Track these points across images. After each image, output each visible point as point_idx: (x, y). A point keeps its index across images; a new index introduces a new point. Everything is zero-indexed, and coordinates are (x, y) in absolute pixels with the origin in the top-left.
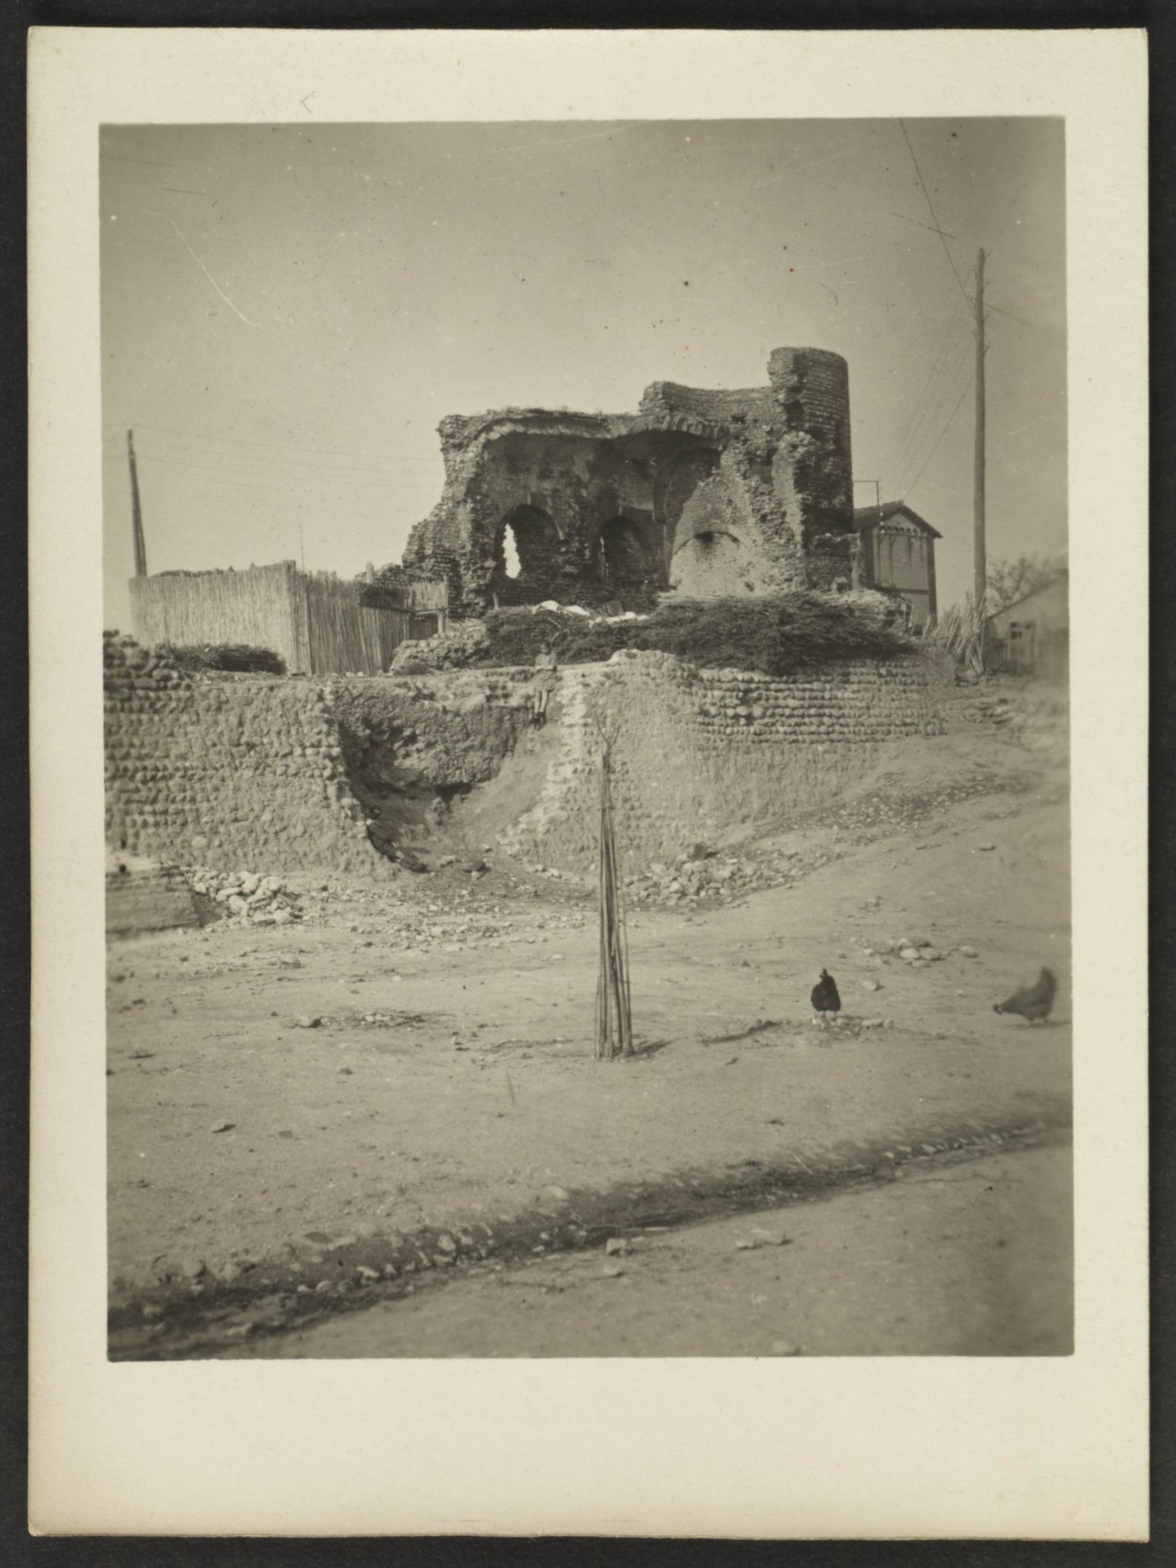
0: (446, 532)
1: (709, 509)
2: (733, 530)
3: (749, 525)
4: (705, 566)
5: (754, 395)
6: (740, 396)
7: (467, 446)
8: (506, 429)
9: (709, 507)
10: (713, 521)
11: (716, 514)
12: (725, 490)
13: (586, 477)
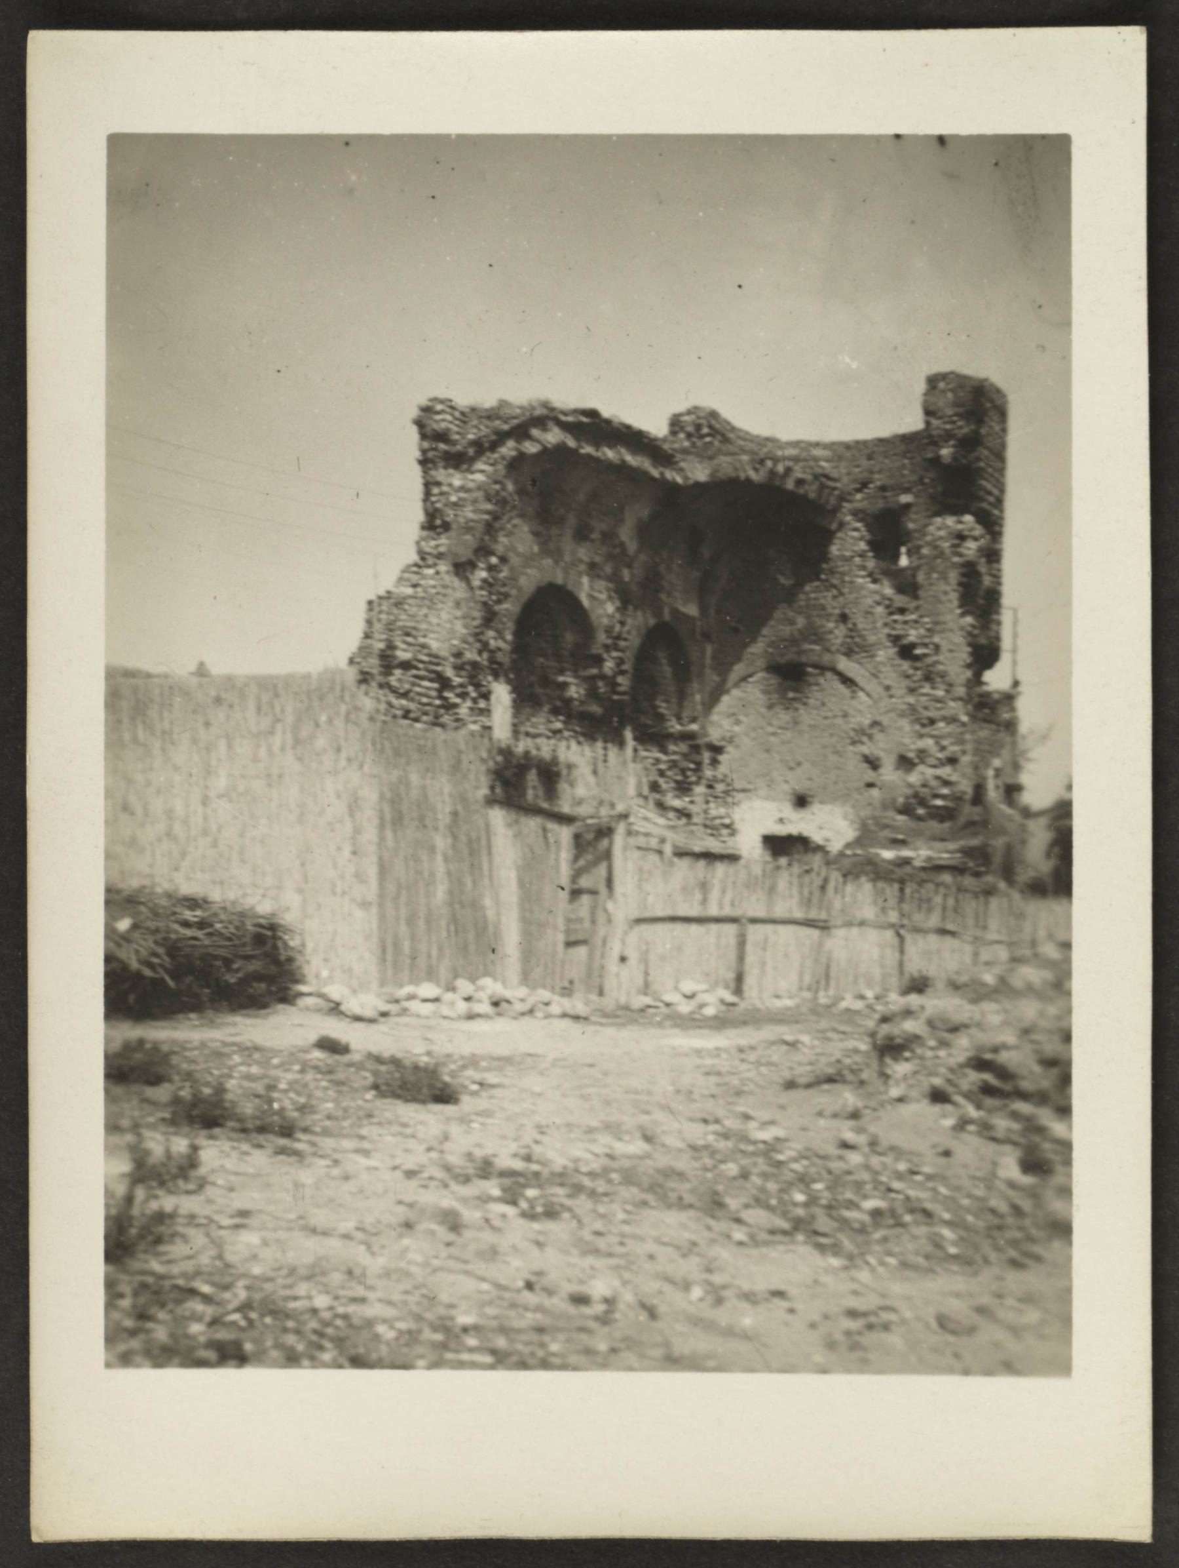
2: (844, 664)
3: (878, 659)
4: (784, 717)
5: (817, 452)
7: (472, 460)
8: (553, 436)
9: (801, 621)
10: (807, 646)
11: (816, 635)
12: (835, 597)
13: (632, 546)
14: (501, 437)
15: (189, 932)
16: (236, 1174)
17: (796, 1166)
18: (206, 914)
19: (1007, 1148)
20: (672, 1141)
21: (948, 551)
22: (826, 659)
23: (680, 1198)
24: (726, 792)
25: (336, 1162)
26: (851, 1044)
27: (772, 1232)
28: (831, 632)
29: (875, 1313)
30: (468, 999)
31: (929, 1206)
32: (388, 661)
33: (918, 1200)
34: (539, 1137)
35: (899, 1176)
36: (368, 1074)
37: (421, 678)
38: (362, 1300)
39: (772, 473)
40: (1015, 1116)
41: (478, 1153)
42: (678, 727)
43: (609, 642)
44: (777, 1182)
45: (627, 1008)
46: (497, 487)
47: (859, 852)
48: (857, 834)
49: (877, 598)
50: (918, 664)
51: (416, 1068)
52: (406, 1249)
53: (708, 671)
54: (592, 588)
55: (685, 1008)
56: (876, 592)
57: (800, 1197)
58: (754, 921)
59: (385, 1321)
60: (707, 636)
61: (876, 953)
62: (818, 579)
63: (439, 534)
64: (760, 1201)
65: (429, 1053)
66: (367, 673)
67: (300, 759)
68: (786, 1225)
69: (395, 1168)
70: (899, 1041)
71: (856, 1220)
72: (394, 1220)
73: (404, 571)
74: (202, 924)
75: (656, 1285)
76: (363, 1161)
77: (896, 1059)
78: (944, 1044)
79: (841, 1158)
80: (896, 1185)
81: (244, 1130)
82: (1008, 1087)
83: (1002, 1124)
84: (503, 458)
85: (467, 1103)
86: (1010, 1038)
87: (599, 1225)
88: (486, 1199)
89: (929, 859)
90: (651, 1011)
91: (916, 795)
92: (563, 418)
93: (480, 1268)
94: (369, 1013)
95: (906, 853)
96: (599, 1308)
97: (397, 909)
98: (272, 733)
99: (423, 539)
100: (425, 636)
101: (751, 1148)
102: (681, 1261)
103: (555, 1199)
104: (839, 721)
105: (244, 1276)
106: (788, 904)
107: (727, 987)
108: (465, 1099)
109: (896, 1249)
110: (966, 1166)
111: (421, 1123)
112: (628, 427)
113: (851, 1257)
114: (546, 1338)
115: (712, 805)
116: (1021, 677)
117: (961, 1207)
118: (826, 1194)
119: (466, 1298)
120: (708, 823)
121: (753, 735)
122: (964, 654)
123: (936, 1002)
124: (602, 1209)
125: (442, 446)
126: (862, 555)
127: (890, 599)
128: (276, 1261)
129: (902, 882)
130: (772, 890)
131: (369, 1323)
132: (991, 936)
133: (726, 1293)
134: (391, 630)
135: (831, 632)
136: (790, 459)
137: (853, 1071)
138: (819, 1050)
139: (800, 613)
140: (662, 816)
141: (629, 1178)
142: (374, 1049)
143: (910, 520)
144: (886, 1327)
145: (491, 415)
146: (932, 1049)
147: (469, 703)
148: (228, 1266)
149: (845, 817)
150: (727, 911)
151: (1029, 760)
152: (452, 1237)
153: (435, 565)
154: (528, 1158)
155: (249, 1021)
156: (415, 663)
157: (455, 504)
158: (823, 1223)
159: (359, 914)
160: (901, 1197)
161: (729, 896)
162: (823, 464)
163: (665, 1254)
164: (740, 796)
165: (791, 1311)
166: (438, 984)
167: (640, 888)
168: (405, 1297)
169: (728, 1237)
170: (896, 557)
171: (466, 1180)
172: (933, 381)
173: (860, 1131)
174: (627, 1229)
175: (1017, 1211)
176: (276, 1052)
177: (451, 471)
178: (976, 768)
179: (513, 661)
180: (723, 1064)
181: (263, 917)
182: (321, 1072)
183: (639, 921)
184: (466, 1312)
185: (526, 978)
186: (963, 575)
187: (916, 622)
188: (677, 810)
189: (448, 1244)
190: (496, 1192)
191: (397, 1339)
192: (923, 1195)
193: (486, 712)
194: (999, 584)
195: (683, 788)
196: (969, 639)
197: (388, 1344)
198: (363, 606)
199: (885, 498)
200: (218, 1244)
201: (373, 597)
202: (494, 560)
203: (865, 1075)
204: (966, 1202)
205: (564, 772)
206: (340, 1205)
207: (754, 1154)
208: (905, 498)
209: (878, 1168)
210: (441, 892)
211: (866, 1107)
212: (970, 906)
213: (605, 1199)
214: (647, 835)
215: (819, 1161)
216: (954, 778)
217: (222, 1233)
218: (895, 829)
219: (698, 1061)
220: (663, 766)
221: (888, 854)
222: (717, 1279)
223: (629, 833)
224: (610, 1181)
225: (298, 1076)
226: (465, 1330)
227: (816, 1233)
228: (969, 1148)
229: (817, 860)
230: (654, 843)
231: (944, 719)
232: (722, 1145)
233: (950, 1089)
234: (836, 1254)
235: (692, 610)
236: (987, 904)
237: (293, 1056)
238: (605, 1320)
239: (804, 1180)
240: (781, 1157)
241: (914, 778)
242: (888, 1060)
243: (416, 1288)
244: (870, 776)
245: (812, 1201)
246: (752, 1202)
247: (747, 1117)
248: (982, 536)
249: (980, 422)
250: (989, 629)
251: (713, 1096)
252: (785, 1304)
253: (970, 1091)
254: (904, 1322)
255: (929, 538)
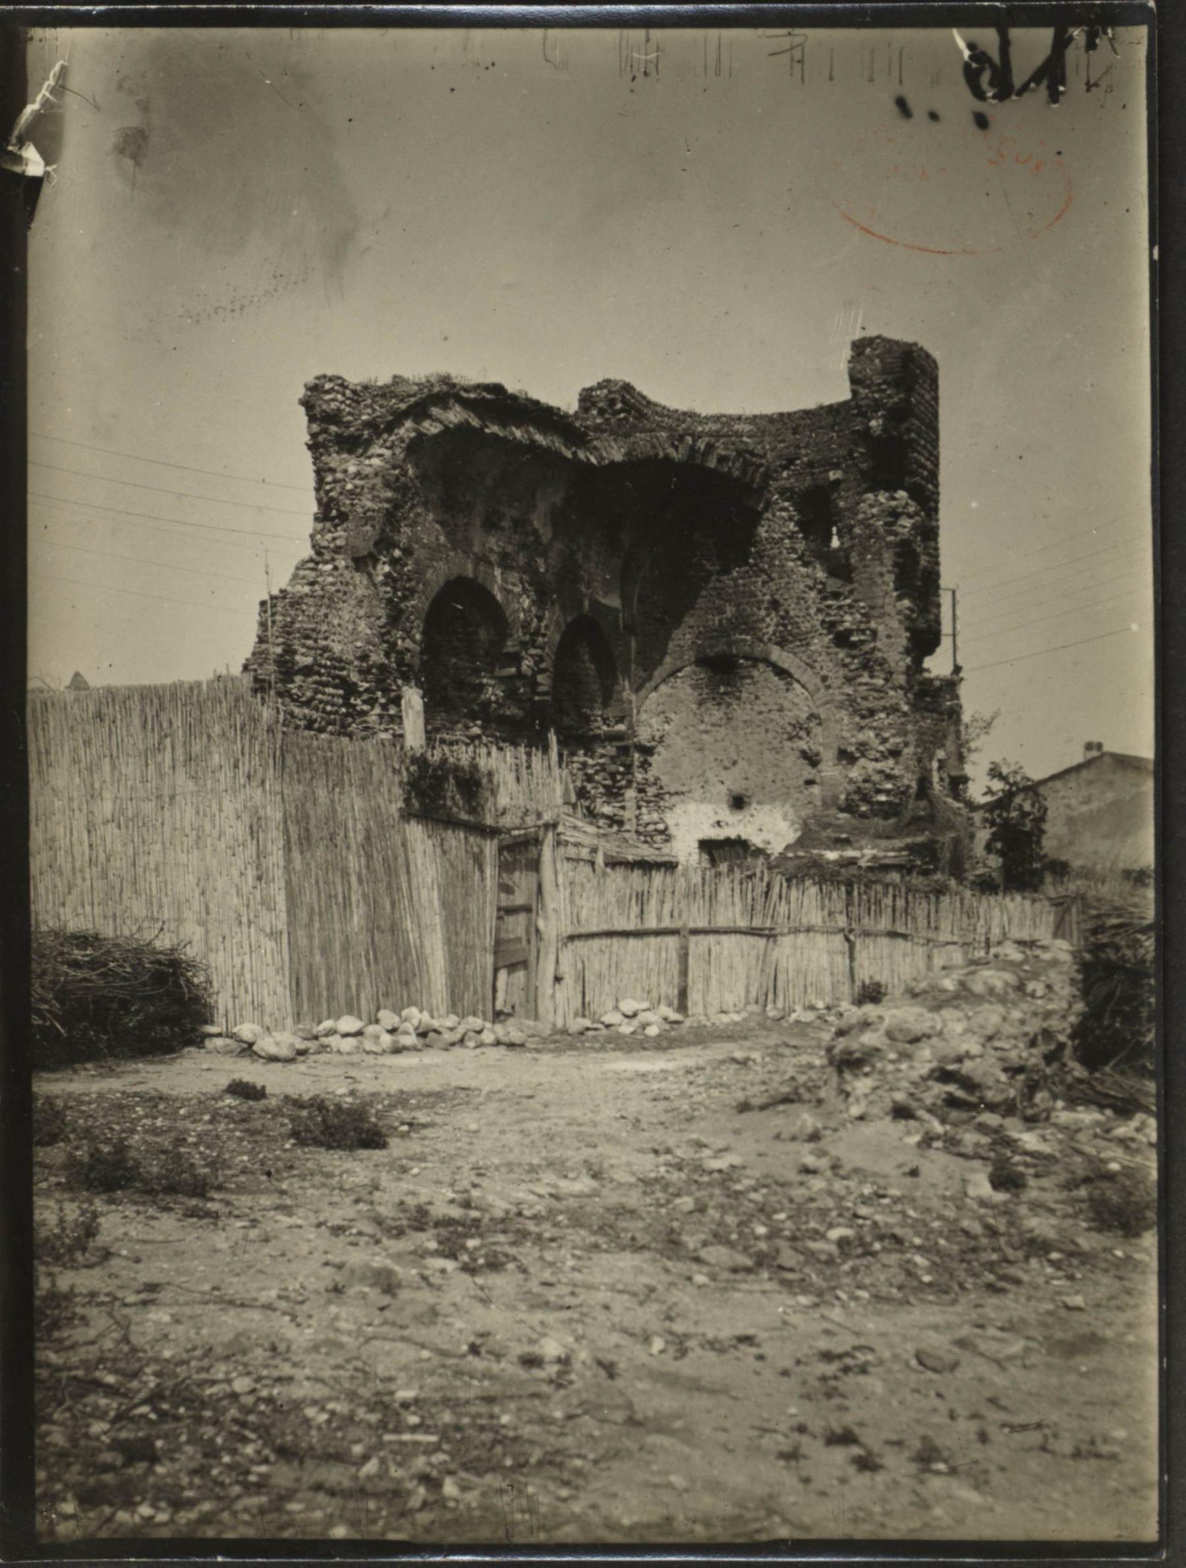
0: (336, 622)
1: (729, 614)
4: (717, 714)
5: (738, 427)
6: (718, 426)
7: (368, 443)
8: (455, 415)
9: (730, 611)
11: (748, 624)
12: (764, 583)
13: (546, 534)
14: (398, 418)
15: (80, 974)
16: (144, 1242)
17: (756, 1196)
18: (98, 954)
19: (977, 1163)
20: (621, 1176)
21: (881, 530)
22: (759, 649)
23: (633, 1239)
24: (659, 796)
25: (254, 1223)
26: (804, 1059)
27: (735, 1270)
28: (763, 620)
29: (847, 1354)
30: (393, 1031)
31: (898, 1231)
32: (287, 668)
33: (887, 1225)
34: (477, 1180)
35: (865, 1201)
36: (286, 1121)
37: (326, 685)
38: (290, 1379)
39: (693, 450)
40: (982, 1128)
41: (411, 1201)
42: (605, 728)
43: (527, 638)
44: (737, 1215)
45: (565, 1031)
46: (397, 472)
47: (801, 854)
48: (799, 834)
49: (810, 582)
50: (855, 652)
51: (339, 1107)
52: (336, 1318)
53: (633, 667)
54: (504, 580)
55: (627, 1029)
56: (808, 576)
57: (761, 1230)
58: (695, 932)
59: (314, 1402)
60: (630, 629)
61: (824, 961)
62: (747, 564)
63: (335, 526)
64: (719, 1237)
65: (352, 1093)
66: (263, 681)
67: (194, 778)
68: (749, 1262)
69: (319, 1225)
70: (857, 1055)
71: (823, 1252)
72: (321, 1286)
73: (297, 568)
74: (93, 964)
75: (615, 1338)
76: (285, 1220)
77: (856, 1076)
78: (905, 1056)
79: (802, 1184)
80: (863, 1210)
81: (150, 1192)
82: (972, 1099)
83: (970, 1138)
84: (402, 440)
85: (397, 1147)
86: (973, 1046)
87: (547, 1275)
88: (421, 1254)
89: (874, 858)
90: (590, 1033)
91: (858, 791)
92: (465, 395)
93: (422, 1333)
94: (284, 1052)
95: (850, 853)
96: (553, 1370)
97: (311, 938)
98: (160, 748)
99: (321, 532)
100: (326, 639)
101: (706, 1179)
102: (640, 1310)
103: (498, 1249)
104: (775, 715)
105: (156, 1360)
106: (731, 913)
107: (670, 1005)
108: (394, 1142)
109: (867, 1281)
110: (934, 1185)
111: (347, 1171)
112: (537, 403)
113: (820, 1294)
114: (496, 1410)
115: (644, 810)
116: (960, 662)
117: (931, 1231)
118: (789, 1224)
119: (405, 1368)
120: (641, 829)
121: (684, 733)
122: (903, 639)
123: (894, 1011)
124: (549, 1256)
125: (333, 429)
126: (792, 536)
127: (824, 584)
128: (189, 1340)
129: (849, 884)
130: (713, 897)
131: (297, 1405)
132: (944, 937)
133: (691, 1343)
134: (289, 633)
135: (763, 620)
136: (710, 434)
137: (809, 1089)
138: (770, 1067)
139: (730, 601)
140: (591, 824)
141: (577, 1220)
142: (293, 1092)
143: (841, 497)
144: (863, 1370)
145: (385, 393)
146: (892, 1062)
147: (377, 710)
148: (134, 1350)
149: (785, 818)
150: (666, 923)
151: (969, 750)
152: (386, 1300)
153: (333, 560)
154: (467, 1205)
155: (150, 1068)
156: (316, 668)
157: (351, 492)
158: (788, 1257)
159: (269, 944)
160: (868, 1222)
161: (667, 907)
162: (745, 439)
163: (620, 1303)
164: (674, 799)
165: (761, 1358)
166: (360, 1017)
167: (572, 902)
168: (335, 1373)
169: (689, 1279)
170: (829, 538)
171: (400, 1233)
172: (859, 347)
173: (822, 1154)
174: (577, 1276)
175: (992, 1232)
176: (185, 1101)
177: (345, 456)
178: (920, 761)
179: (422, 662)
180: (671, 1088)
181: (161, 953)
182: (235, 1122)
183: (572, 938)
184: (407, 1386)
185: (455, 1004)
186: (898, 555)
187: (850, 606)
188: (607, 817)
189: (382, 1309)
190: (433, 1245)
191: (329, 1422)
192: (892, 1220)
193: (397, 719)
194: (937, 564)
195: (613, 793)
196: (907, 623)
197: (319, 1428)
198: (257, 608)
199: (813, 474)
200: (125, 1326)
201: (266, 597)
202: (397, 553)
203: (822, 1094)
204: (936, 1224)
205: (484, 781)
206: (261, 1271)
207: (710, 1184)
208: (833, 475)
209: (843, 1193)
210: (357, 918)
211: (825, 1128)
212: (921, 909)
213: (554, 1245)
214: (576, 845)
215: (779, 1189)
216: (896, 772)
217: (127, 1311)
218: (840, 828)
219: (645, 1086)
220: (590, 771)
221: (832, 855)
222: (679, 1327)
223: (558, 843)
224: (556, 1225)
225: (210, 1127)
226: (405, 1405)
227: (781, 1268)
228: (937, 1164)
229: (760, 863)
230: (585, 853)
231: (884, 709)
232: (675, 1176)
233: (913, 1104)
234: (804, 1292)
235: (614, 601)
236: (937, 902)
237: (204, 1103)
238: (558, 1383)
239: (764, 1211)
240: (738, 1187)
241: (855, 773)
242: (848, 1076)
243: (348, 1361)
244: (809, 772)
245: (774, 1233)
246: (710, 1238)
247: (700, 1145)
248: (917, 514)
249: (910, 390)
250: (929, 612)
251: (662, 1123)
252: (753, 1351)
253: (934, 1105)
254: (881, 1362)
255: (861, 516)
